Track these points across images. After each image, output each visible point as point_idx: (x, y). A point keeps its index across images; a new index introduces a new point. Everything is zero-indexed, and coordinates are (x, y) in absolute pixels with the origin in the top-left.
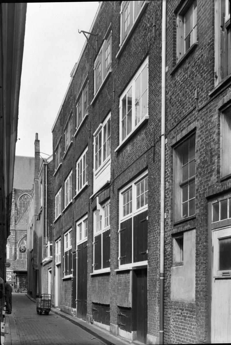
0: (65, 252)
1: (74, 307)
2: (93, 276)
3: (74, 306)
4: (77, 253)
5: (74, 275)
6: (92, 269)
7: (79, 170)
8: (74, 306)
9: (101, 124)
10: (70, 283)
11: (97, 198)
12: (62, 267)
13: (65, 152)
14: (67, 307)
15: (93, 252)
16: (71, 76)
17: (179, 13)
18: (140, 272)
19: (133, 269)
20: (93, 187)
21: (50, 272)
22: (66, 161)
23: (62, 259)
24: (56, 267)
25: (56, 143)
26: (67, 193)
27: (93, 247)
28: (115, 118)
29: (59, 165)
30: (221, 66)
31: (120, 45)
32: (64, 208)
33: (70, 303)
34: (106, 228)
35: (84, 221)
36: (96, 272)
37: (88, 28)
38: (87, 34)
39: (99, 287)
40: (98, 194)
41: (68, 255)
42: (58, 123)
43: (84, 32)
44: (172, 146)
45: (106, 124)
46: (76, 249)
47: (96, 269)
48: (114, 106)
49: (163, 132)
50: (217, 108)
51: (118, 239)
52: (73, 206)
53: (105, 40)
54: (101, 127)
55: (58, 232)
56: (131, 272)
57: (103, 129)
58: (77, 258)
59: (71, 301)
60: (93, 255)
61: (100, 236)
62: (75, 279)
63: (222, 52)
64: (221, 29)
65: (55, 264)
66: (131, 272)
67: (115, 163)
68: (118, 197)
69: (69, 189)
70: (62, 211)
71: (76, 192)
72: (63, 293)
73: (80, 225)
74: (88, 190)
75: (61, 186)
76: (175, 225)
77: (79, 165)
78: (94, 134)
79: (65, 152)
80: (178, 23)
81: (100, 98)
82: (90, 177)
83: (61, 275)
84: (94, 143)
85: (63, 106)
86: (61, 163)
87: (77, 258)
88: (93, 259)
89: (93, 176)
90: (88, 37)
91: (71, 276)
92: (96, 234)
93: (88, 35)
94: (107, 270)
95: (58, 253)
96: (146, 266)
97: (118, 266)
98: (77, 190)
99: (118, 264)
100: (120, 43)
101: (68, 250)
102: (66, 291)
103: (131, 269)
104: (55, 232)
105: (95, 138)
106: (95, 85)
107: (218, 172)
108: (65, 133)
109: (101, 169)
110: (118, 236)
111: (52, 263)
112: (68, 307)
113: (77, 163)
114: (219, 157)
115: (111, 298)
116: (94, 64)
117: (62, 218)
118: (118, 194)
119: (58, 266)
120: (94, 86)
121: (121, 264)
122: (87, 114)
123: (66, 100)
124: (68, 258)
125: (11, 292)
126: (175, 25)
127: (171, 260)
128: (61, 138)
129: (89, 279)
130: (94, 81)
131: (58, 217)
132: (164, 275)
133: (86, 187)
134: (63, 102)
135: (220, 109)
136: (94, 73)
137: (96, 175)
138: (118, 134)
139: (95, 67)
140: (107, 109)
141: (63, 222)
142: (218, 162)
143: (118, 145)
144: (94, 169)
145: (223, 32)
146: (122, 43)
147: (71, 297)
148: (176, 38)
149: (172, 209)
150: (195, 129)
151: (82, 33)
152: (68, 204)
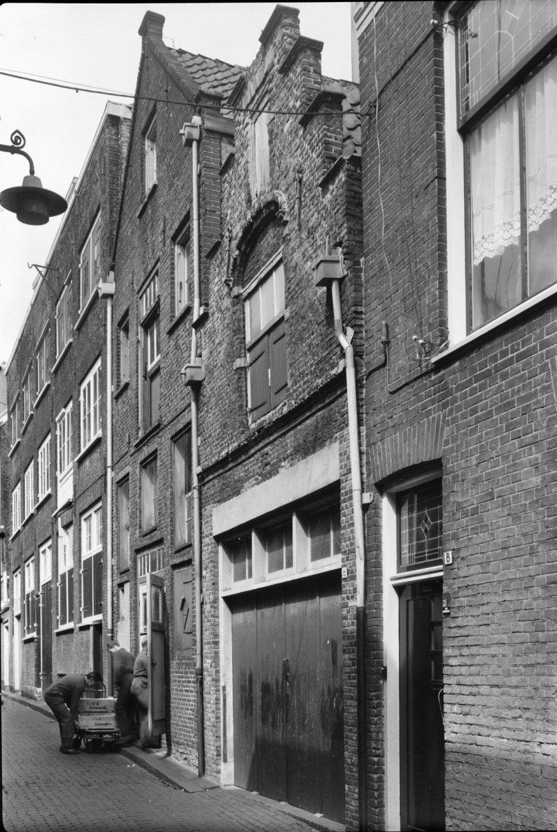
0: (83, 559)
1: (39, 686)
2: (59, 634)
3: (38, 685)
4: (41, 596)
5: (38, 633)
6: (58, 624)
7: (85, 402)
8: (38, 685)
9: (63, 410)
10: (33, 645)
11: (59, 519)
12: (22, 619)
13: (24, 422)
14: (29, 687)
15: (57, 597)
16: (34, 289)
17: (122, 327)
18: (98, 628)
19: (95, 623)
20: (56, 498)
21: (7, 628)
22: (28, 435)
23: (23, 607)
24: (15, 619)
25: (12, 399)
26: (87, 413)
27: (57, 590)
28: (76, 412)
29: (66, 346)
30: (144, 418)
31: (80, 312)
32: (24, 518)
33: (33, 681)
34: (88, 553)
35: (49, 547)
36: (62, 628)
37: (44, 259)
38: (41, 269)
39: (64, 650)
40: (60, 513)
41: (30, 599)
42: (14, 366)
43: (36, 266)
44: (117, 483)
45: (96, 374)
46: (39, 591)
47: (61, 624)
48: (75, 394)
49: (109, 463)
50: (139, 461)
51: (81, 583)
52: (35, 520)
53: (66, 286)
54: (64, 414)
55: (16, 559)
56: (92, 628)
57: (66, 417)
58: (41, 605)
59: (34, 676)
60: (57, 602)
61: (65, 574)
62: (39, 639)
63: (144, 403)
64: (143, 379)
65: (13, 614)
66: (92, 628)
67: (77, 477)
68: (80, 524)
69: (46, 467)
70: (73, 459)
71: (38, 498)
72: (25, 662)
73: (44, 552)
74: (52, 500)
75: (20, 479)
76: (121, 574)
77: (84, 391)
78: (57, 419)
79: (25, 423)
80: (121, 339)
81: (67, 362)
82: (54, 482)
83: (23, 634)
84: (81, 399)
85: (20, 340)
86: (71, 340)
87: (41, 605)
88: (57, 609)
89: (56, 482)
90: (43, 273)
91: (34, 635)
92: (61, 571)
93: (43, 271)
94: (69, 625)
95: (17, 595)
96: (101, 621)
97: (81, 619)
98: (40, 495)
99: (81, 617)
100: (79, 308)
101: (92, 555)
102: (28, 662)
103: (92, 624)
104: (12, 556)
105: (58, 425)
106: (57, 342)
107: (140, 527)
108: (56, 317)
109: (65, 476)
110: (80, 578)
111: (9, 613)
112: (31, 687)
113: (82, 388)
114: (140, 512)
115: (75, 665)
116: (56, 308)
117: (21, 534)
118: (80, 521)
119: (18, 617)
120: (56, 343)
121: (85, 617)
122: (49, 383)
123: (24, 335)
124: (31, 604)
125: (117, 704)
126: (118, 340)
127: (118, 614)
128: (19, 395)
129: (54, 637)
130: (56, 335)
131: (17, 531)
132: (112, 631)
133: (49, 496)
134: (62, 225)
135: (141, 463)
136: (56, 323)
137: (60, 481)
138: (80, 437)
139: (81, 263)
140: (45, 431)
141: (24, 543)
142: (140, 517)
143: (79, 452)
144: (58, 473)
145: (146, 382)
146: (83, 309)
147: (33, 669)
148: (120, 355)
149: (118, 554)
150: (128, 474)
151: (34, 267)
152: (89, 440)
